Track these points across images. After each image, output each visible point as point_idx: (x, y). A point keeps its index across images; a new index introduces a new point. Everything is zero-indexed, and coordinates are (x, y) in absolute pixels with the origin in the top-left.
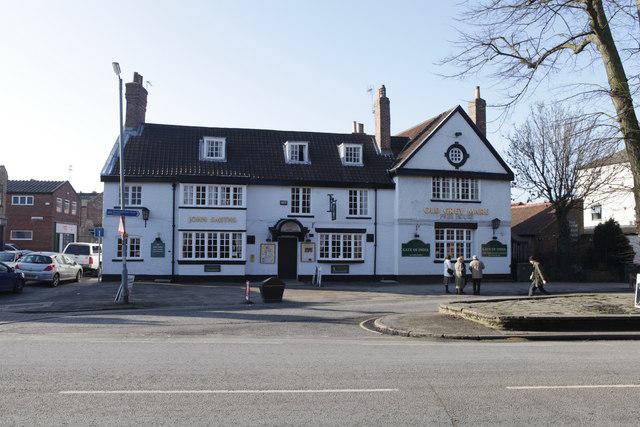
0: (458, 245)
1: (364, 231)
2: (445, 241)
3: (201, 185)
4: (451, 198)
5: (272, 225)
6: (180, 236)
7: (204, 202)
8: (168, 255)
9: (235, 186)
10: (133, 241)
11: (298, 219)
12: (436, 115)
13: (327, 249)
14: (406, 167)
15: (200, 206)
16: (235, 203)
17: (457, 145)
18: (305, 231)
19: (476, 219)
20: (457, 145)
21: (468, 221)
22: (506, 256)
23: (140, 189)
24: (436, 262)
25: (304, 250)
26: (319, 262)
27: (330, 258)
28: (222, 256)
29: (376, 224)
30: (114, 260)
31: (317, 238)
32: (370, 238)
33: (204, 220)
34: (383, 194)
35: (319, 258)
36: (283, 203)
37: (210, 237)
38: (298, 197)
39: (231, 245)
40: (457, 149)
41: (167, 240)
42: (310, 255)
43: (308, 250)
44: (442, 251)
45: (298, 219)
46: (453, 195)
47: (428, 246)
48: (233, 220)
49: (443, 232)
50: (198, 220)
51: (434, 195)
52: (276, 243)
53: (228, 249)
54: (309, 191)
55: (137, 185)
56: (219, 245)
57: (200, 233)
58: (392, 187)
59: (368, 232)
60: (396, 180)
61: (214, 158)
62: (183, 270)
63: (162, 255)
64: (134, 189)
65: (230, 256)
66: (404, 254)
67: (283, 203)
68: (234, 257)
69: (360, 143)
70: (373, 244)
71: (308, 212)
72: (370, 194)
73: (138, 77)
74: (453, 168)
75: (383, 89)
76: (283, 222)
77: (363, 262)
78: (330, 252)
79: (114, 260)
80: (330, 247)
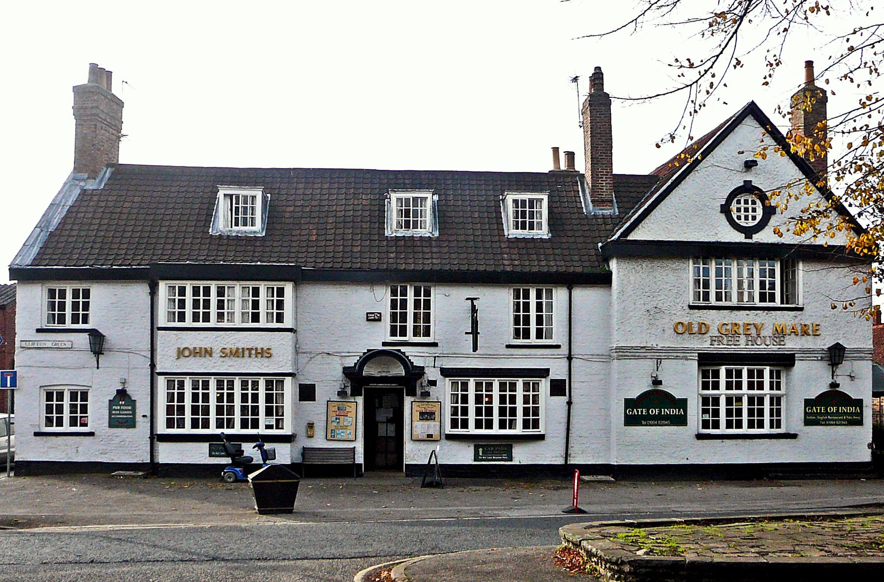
0: (751, 400)
1: (544, 373)
2: (723, 391)
3: (202, 284)
4: (734, 302)
5: (351, 362)
6: (161, 382)
7: (207, 318)
8: (143, 425)
9: (221, 283)
10: (73, 396)
11: (403, 349)
12: (728, 118)
13: (465, 411)
14: (632, 237)
15: (201, 324)
16: (539, 335)
17: (748, 188)
18: (415, 374)
19: (791, 344)
20: (748, 188)
21: (773, 348)
22: (860, 423)
23: (87, 293)
24: (700, 437)
25: (417, 415)
26: (450, 437)
27: (472, 430)
28: (244, 425)
29: (570, 358)
30: (37, 434)
31: (444, 390)
32: (558, 388)
33: (208, 352)
34: (584, 296)
35: (448, 430)
36: (374, 318)
37: (195, 387)
38: (404, 303)
39: (262, 404)
40: (734, 206)
41: (139, 393)
42: (432, 427)
43: (427, 416)
44: (716, 413)
45: (403, 349)
46: (740, 294)
47: (683, 403)
48: (264, 353)
49: (716, 374)
50: (197, 353)
51: (697, 296)
52: (360, 400)
53: (255, 411)
54: (428, 293)
55: (81, 286)
56: (237, 403)
57: (201, 380)
58: (604, 280)
59: (553, 376)
60: (613, 265)
61: (241, 228)
62: (168, 454)
63: (130, 423)
64: (76, 293)
65: (262, 424)
66: (630, 421)
67: (374, 318)
68: (269, 427)
69: (541, 191)
70: (564, 399)
71: (427, 333)
72: (560, 295)
73: (99, 75)
74: (739, 238)
75: (597, 77)
76: (371, 356)
77: (541, 437)
78: (472, 417)
79: (37, 434)
80: (472, 406)
